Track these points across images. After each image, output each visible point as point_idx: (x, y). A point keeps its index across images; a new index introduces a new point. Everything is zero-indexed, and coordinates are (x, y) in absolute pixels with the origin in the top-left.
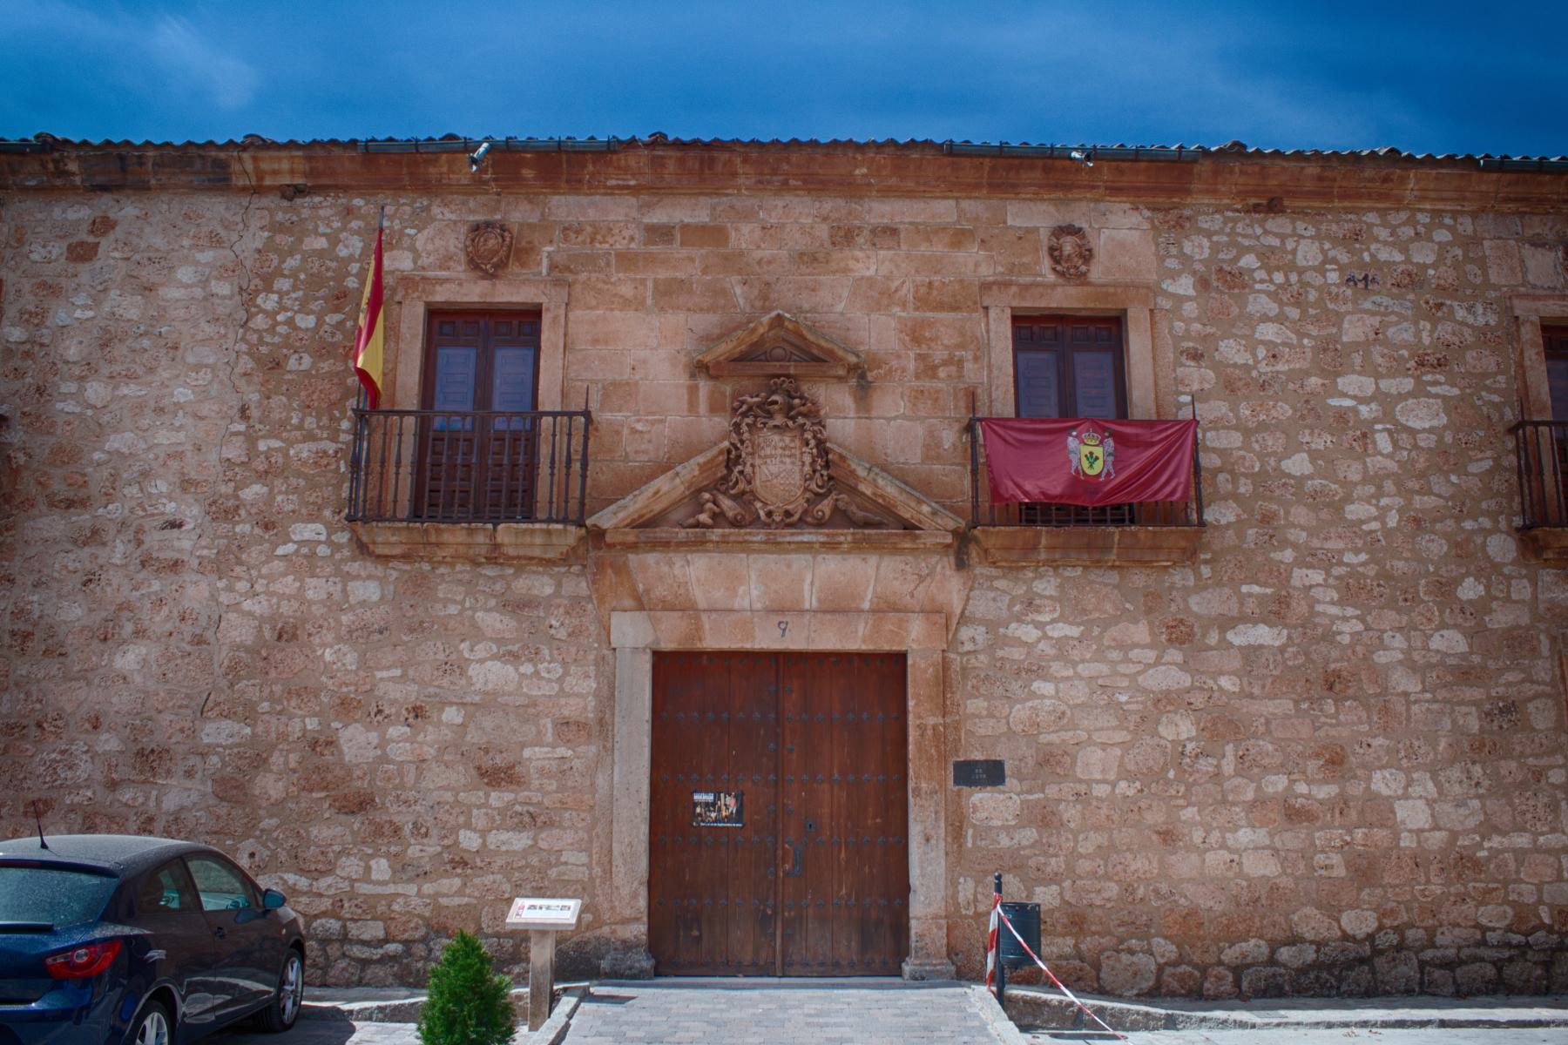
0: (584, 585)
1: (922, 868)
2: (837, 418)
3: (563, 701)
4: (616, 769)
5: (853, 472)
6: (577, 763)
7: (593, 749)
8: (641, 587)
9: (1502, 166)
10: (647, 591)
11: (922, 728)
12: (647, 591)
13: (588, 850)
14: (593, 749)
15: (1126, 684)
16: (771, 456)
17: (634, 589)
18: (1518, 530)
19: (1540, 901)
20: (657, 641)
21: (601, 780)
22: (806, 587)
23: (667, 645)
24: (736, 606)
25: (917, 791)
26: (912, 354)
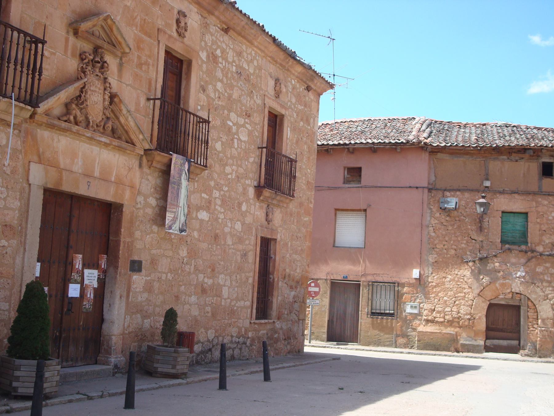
0: (19, 142)
1: (118, 311)
2: (112, 78)
3: (6, 212)
4: (26, 254)
5: (121, 110)
6: (9, 250)
7: (15, 242)
8: (41, 150)
9: (23, 267)
10: (43, 153)
11: (124, 242)
12: (43, 153)
13: (9, 302)
14: (15, 242)
15: (172, 359)
16: (95, 91)
17: (38, 151)
18: (255, 187)
19: (243, 326)
20: (46, 183)
21: (18, 260)
22: (96, 165)
23: (50, 186)
24: (73, 170)
25: (120, 273)
26: (136, 54)
